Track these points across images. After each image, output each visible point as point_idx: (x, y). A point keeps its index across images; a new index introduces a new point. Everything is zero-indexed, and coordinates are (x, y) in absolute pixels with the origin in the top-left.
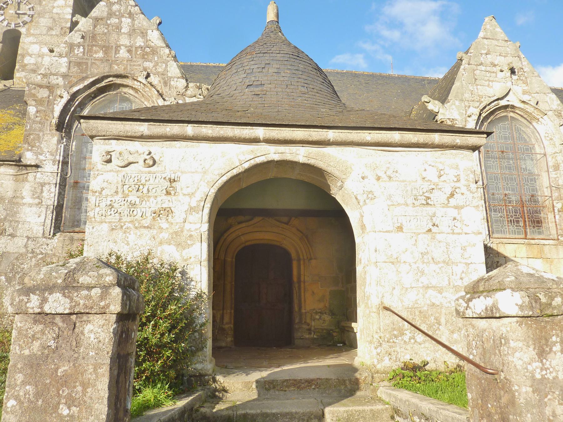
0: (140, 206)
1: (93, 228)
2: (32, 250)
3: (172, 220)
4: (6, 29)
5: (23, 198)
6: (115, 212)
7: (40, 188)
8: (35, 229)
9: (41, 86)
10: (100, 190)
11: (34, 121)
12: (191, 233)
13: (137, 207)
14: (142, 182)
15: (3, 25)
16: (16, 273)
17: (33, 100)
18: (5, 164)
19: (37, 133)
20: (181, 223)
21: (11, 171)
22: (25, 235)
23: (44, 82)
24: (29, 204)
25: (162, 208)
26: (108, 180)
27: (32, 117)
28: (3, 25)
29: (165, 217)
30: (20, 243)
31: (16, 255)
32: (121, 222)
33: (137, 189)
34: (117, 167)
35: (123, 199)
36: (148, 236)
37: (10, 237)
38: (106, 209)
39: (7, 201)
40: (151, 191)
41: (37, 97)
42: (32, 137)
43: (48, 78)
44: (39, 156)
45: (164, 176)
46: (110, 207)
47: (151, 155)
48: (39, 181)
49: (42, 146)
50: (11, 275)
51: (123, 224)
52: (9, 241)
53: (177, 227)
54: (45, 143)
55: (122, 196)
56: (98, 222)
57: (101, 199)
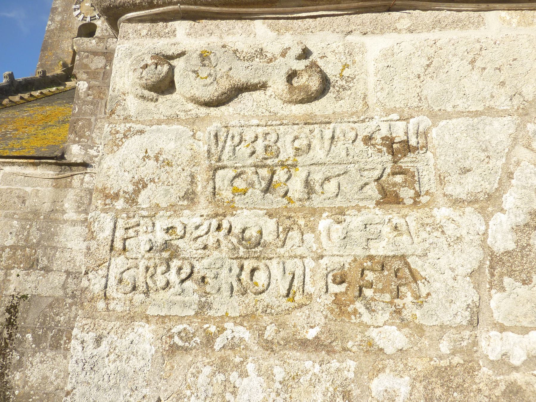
0: (282, 251)
1: (98, 341)
2: (73, 292)
3: (418, 313)
4: (82, 24)
5: (64, 212)
6: (183, 276)
7: (88, 196)
8: (78, 259)
9: (95, 53)
10: (131, 188)
11: (84, 101)
12: (515, 376)
13: (268, 253)
14: (282, 157)
15: (79, 19)
16: (48, 329)
17: (84, 72)
18: (43, 163)
19: (87, 118)
20: (459, 328)
21: (50, 172)
22: (64, 268)
23: (100, 48)
24: (73, 221)
25: (371, 258)
26: (160, 153)
27: (82, 96)
28: (79, 19)
29: (387, 297)
30: (57, 281)
31: (50, 300)
32: (207, 320)
33: (264, 184)
34: (191, 106)
35: (215, 223)
36: (320, 388)
37: (42, 272)
38: (151, 264)
39: (42, 217)
40: (317, 188)
41: (90, 68)
42: (80, 124)
43: (105, 42)
44: (89, 150)
45: (364, 130)
46: (166, 255)
47: (311, 58)
48: (87, 186)
49: (94, 135)
50: (40, 333)
51: (213, 329)
52: (41, 277)
53: (445, 347)
54: (98, 131)
55: (209, 211)
56: (118, 318)
57: (133, 221)
